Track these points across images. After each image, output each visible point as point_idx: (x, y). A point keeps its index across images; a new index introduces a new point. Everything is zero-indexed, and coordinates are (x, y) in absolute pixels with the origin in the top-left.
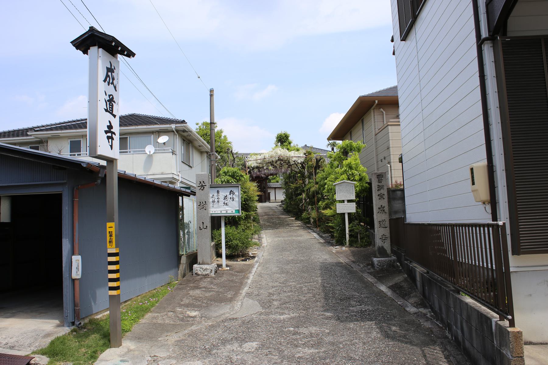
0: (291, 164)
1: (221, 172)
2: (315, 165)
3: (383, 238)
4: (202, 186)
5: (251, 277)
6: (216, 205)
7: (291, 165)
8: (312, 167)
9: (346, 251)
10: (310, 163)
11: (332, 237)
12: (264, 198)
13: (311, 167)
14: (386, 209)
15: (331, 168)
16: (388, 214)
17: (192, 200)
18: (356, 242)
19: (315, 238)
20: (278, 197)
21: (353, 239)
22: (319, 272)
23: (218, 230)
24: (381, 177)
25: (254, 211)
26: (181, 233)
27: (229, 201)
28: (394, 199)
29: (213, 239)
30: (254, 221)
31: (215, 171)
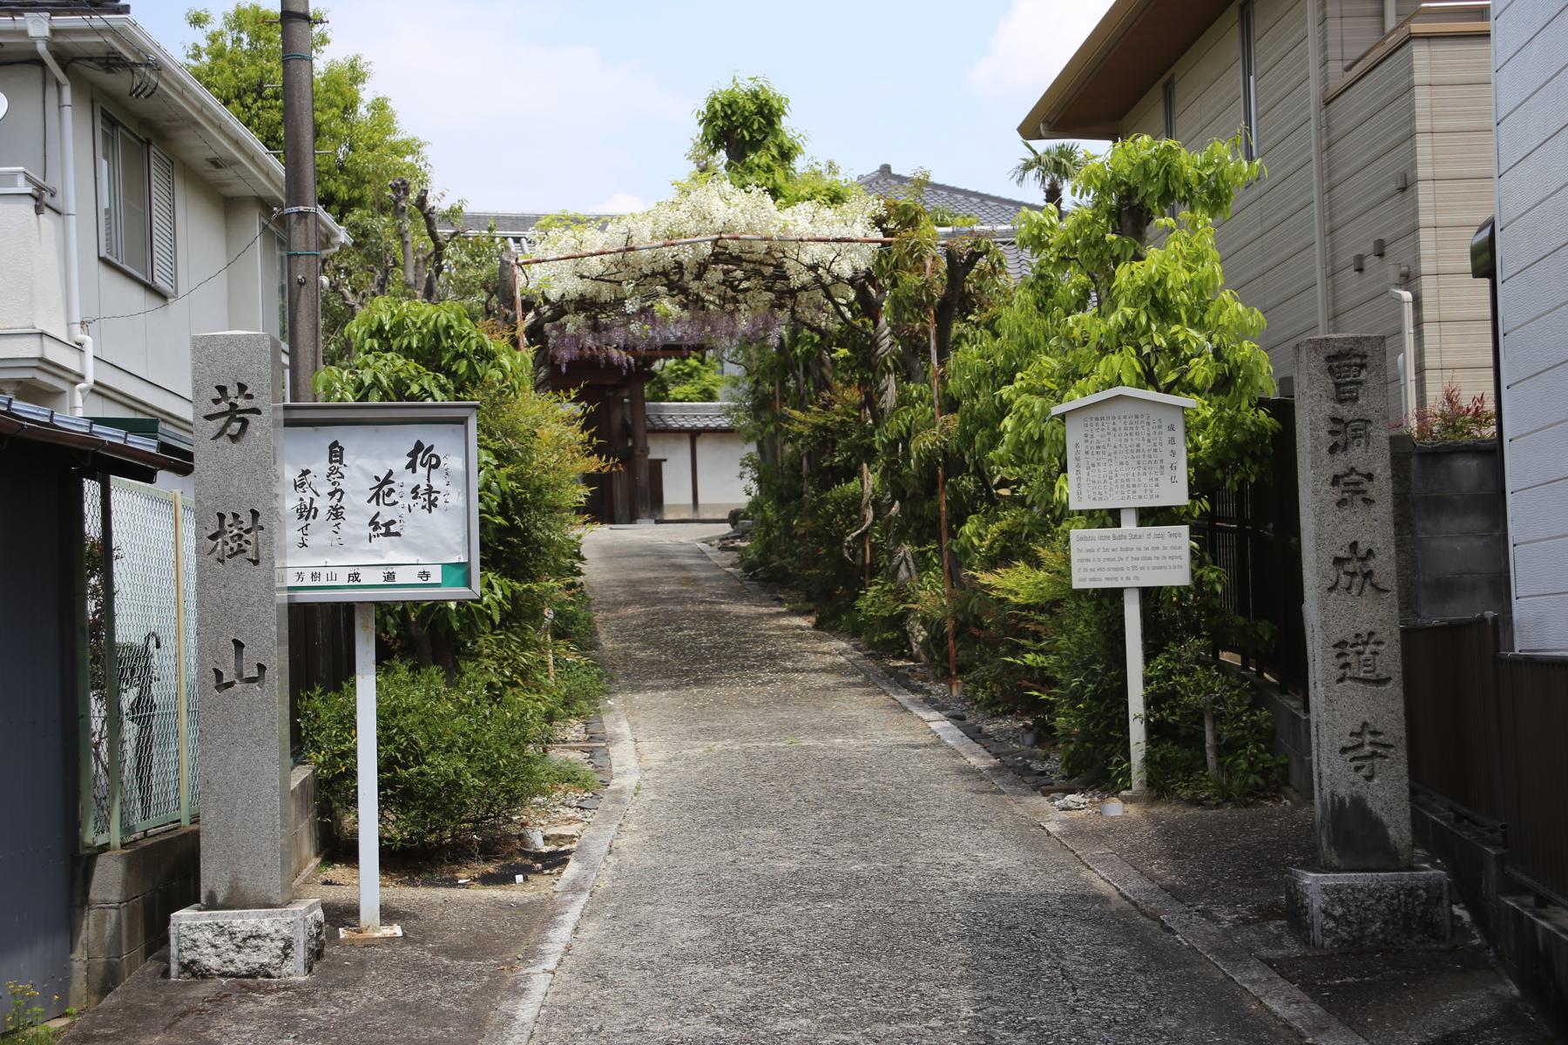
0: (795, 283)
1: (355, 328)
2: (939, 291)
3: (1364, 748)
4: (234, 417)
5: (539, 982)
6: (321, 531)
7: (793, 293)
8: (919, 304)
9: (1132, 826)
10: (911, 280)
11: (1044, 735)
12: (626, 492)
14: (1385, 566)
15: (1042, 308)
16: (1392, 598)
17: (172, 504)
19: (938, 743)
20: (713, 487)
21: (1168, 748)
22: (960, 953)
23: (338, 689)
24: (1352, 365)
25: (559, 572)
26: (97, 710)
27: (402, 508)
28: (1438, 505)
29: (299, 744)
30: (559, 634)
31: (313, 318)
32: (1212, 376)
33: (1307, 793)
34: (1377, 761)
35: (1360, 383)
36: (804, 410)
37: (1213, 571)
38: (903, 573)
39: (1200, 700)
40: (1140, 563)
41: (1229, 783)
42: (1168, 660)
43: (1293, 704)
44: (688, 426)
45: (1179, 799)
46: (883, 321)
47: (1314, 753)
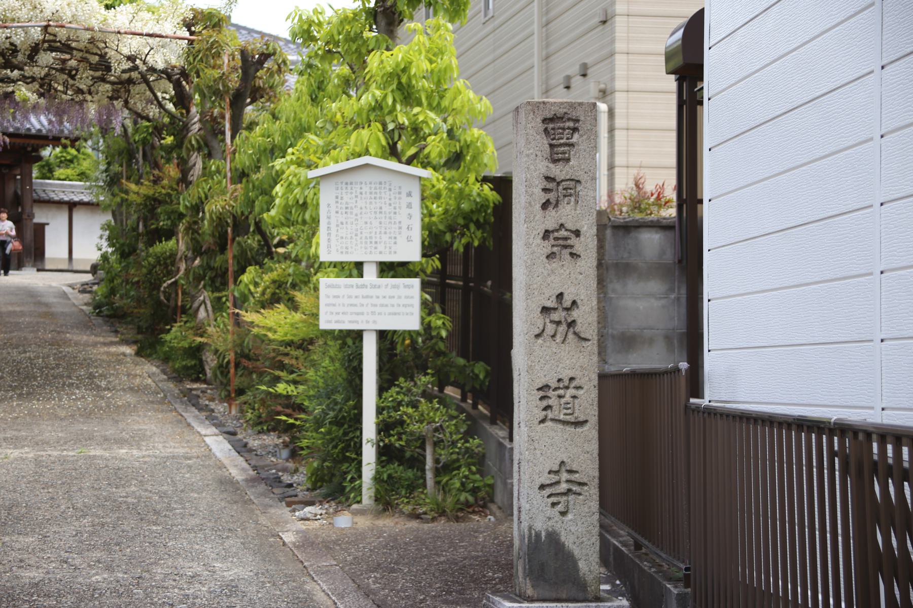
3: (559, 487)
8: (217, 93)
13: (214, 92)
14: (586, 317)
15: (314, 100)
16: (592, 346)
18: (414, 486)
21: (395, 469)
28: (625, 269)
32: (445, 152)
33: (507, 511)
34: (571, 497)
35: (572, 145)
36: (138, 183)
37: (440, 318)
38: (202, 314)
39: (424, 428)
40: (378, 309)
41: (444, 500)
42: (398, 393)
43: (499, 432)
44: (66, 199)
45: (402, 513)
46: (194, 110)
47: (515, 475)
